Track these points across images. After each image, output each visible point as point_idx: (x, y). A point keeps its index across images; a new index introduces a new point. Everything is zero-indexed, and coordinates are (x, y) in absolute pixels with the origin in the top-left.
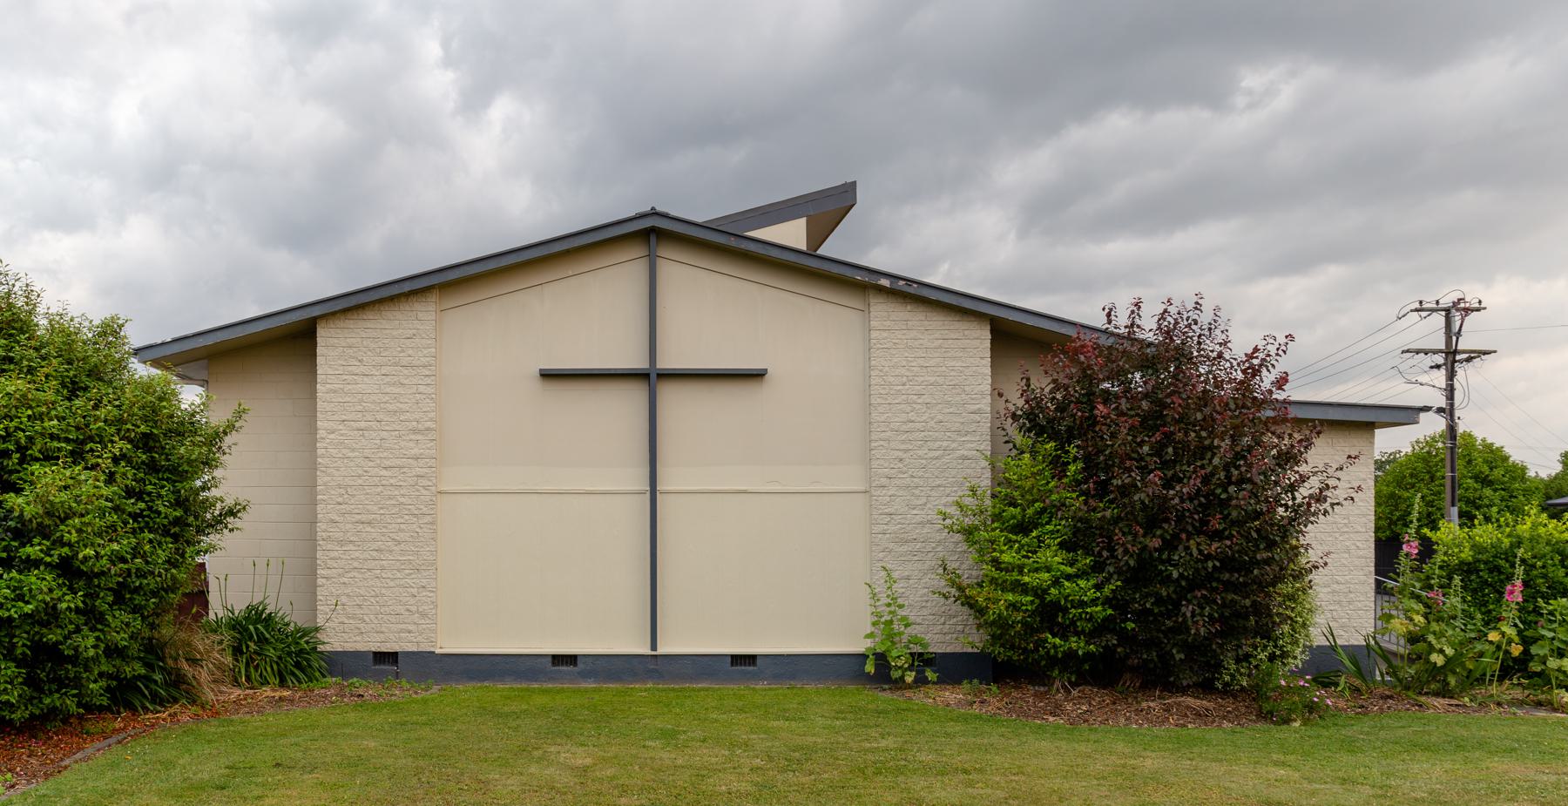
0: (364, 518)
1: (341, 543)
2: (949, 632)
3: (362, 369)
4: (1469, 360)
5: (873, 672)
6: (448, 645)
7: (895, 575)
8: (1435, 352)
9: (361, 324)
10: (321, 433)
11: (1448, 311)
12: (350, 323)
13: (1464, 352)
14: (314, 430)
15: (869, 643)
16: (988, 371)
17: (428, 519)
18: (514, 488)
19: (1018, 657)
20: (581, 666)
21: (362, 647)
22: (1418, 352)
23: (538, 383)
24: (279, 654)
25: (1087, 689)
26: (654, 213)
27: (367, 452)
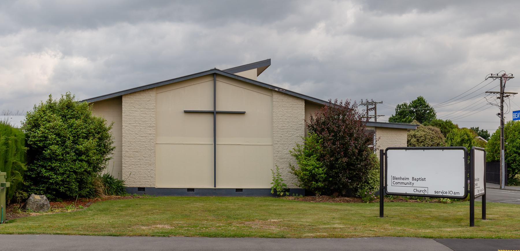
0: (135, 150)
1: (129, 157)
2: (292, 183)
3: (135, 109)
4: (507, 96)
5: (275, 193)
6: (159, 185)
7: (279, 168)
8: (497, 93)
9: (135, 97)
10: (123, 127)
11: (501, 78)
12: (132, 97)
13: (506, 93)
14: (122, 126)
15: (272, 185)
16: (304, 113)
17: (153, 151)
18: (177, 143)
19: (311, 188)
20: (195, 191)
21: (135, 186)
22: (491, 93)
23: (183, 114)
24: (116, 188)
25: (324, 196)
26: (215, 69)
27: (136, 132)
